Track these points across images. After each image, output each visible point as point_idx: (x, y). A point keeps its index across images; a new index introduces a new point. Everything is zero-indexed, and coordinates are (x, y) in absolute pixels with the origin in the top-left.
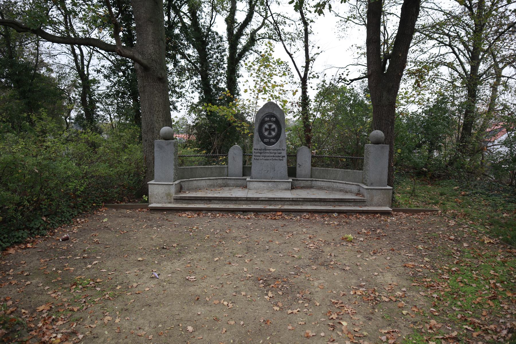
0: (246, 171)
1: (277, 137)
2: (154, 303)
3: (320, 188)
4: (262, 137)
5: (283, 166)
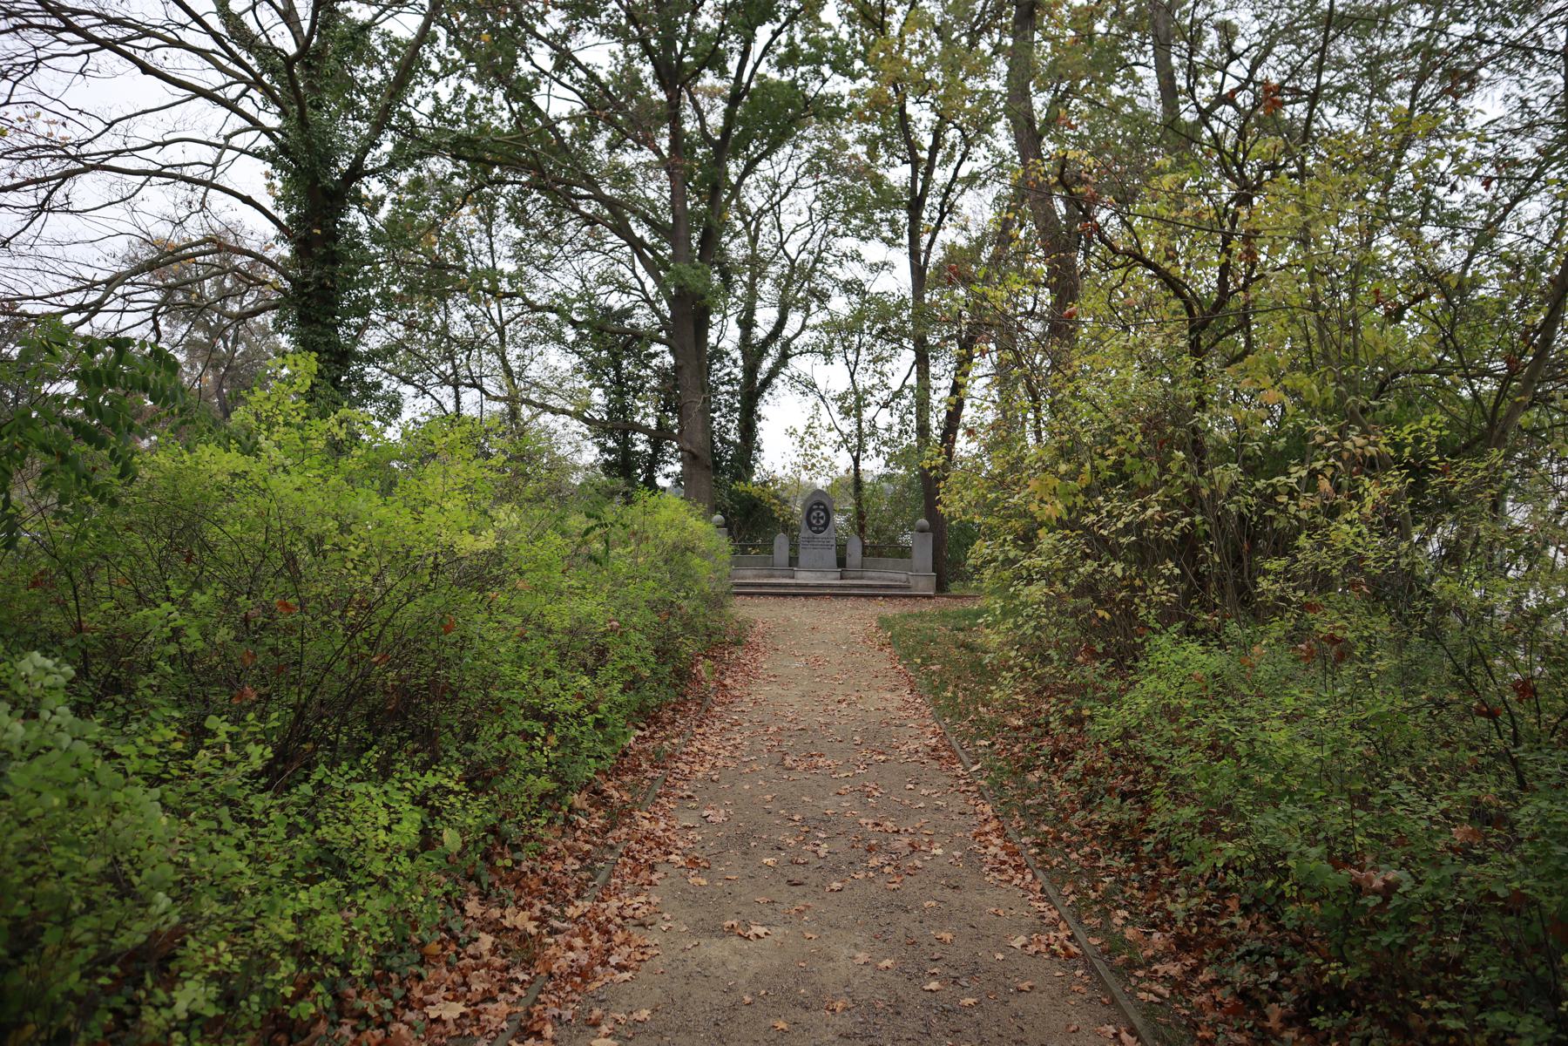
0: (793, 561)
1: (826, 525)
2: (1241, 572)
3: (871, 579)
4: (810, 525)
5: (831, 556)
